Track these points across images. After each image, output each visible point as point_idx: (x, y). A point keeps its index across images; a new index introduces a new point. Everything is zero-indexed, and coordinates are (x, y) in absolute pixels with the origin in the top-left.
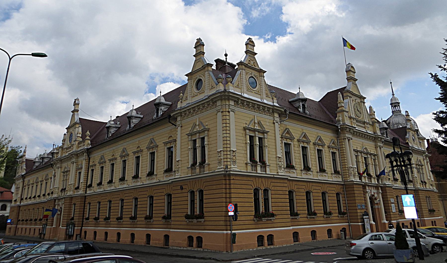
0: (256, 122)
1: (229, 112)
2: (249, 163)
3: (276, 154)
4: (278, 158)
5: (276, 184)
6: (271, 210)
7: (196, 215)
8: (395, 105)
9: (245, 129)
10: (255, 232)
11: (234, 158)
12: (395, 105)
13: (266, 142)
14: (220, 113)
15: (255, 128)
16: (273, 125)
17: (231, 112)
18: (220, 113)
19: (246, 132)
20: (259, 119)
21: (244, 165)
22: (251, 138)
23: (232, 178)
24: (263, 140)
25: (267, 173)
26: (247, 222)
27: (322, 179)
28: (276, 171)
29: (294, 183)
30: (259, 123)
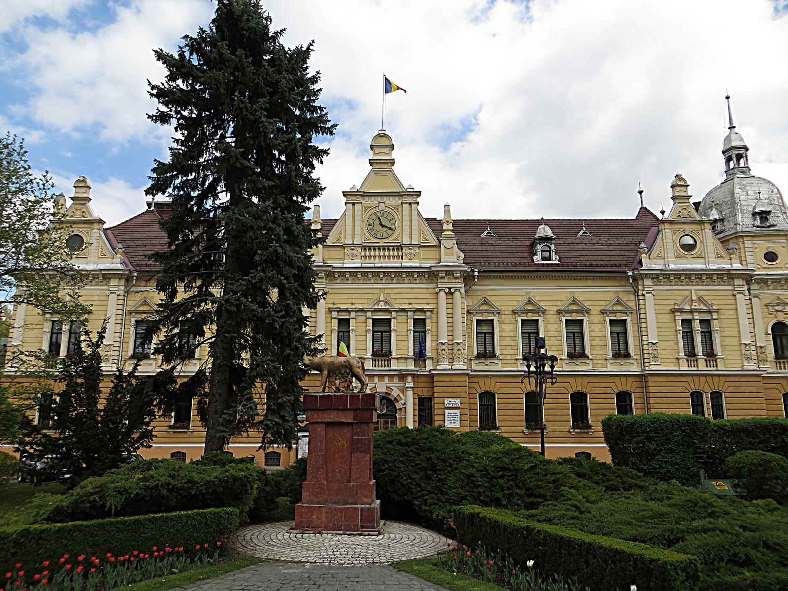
0: (694, 298)
1: (643, 295)
2: (682, 358)
3: (740, 340)
4: (743, 346)
5: (597, 385)
6: (590, 422)
7: (71, 418)
8: (735, 154)
9: (673, 312)
10: (168, 448)
11: (655, 352)
12: (735, 154)
13: (715, 326)
14: (115, 295)
15: (693, 307)
16: (733, 298)
17: (647, 295)
18: (115, 295)
19: (675, 316)
20: (700, 294)
21: (675, 361)
22: (687, 323)
23: (649, 379)
24: (711, 322)
25: (719, 369)
26: (561, 434)
27: (617, 369)
28: (740, 365)
29: (722, 379)
30: (701, 300)
